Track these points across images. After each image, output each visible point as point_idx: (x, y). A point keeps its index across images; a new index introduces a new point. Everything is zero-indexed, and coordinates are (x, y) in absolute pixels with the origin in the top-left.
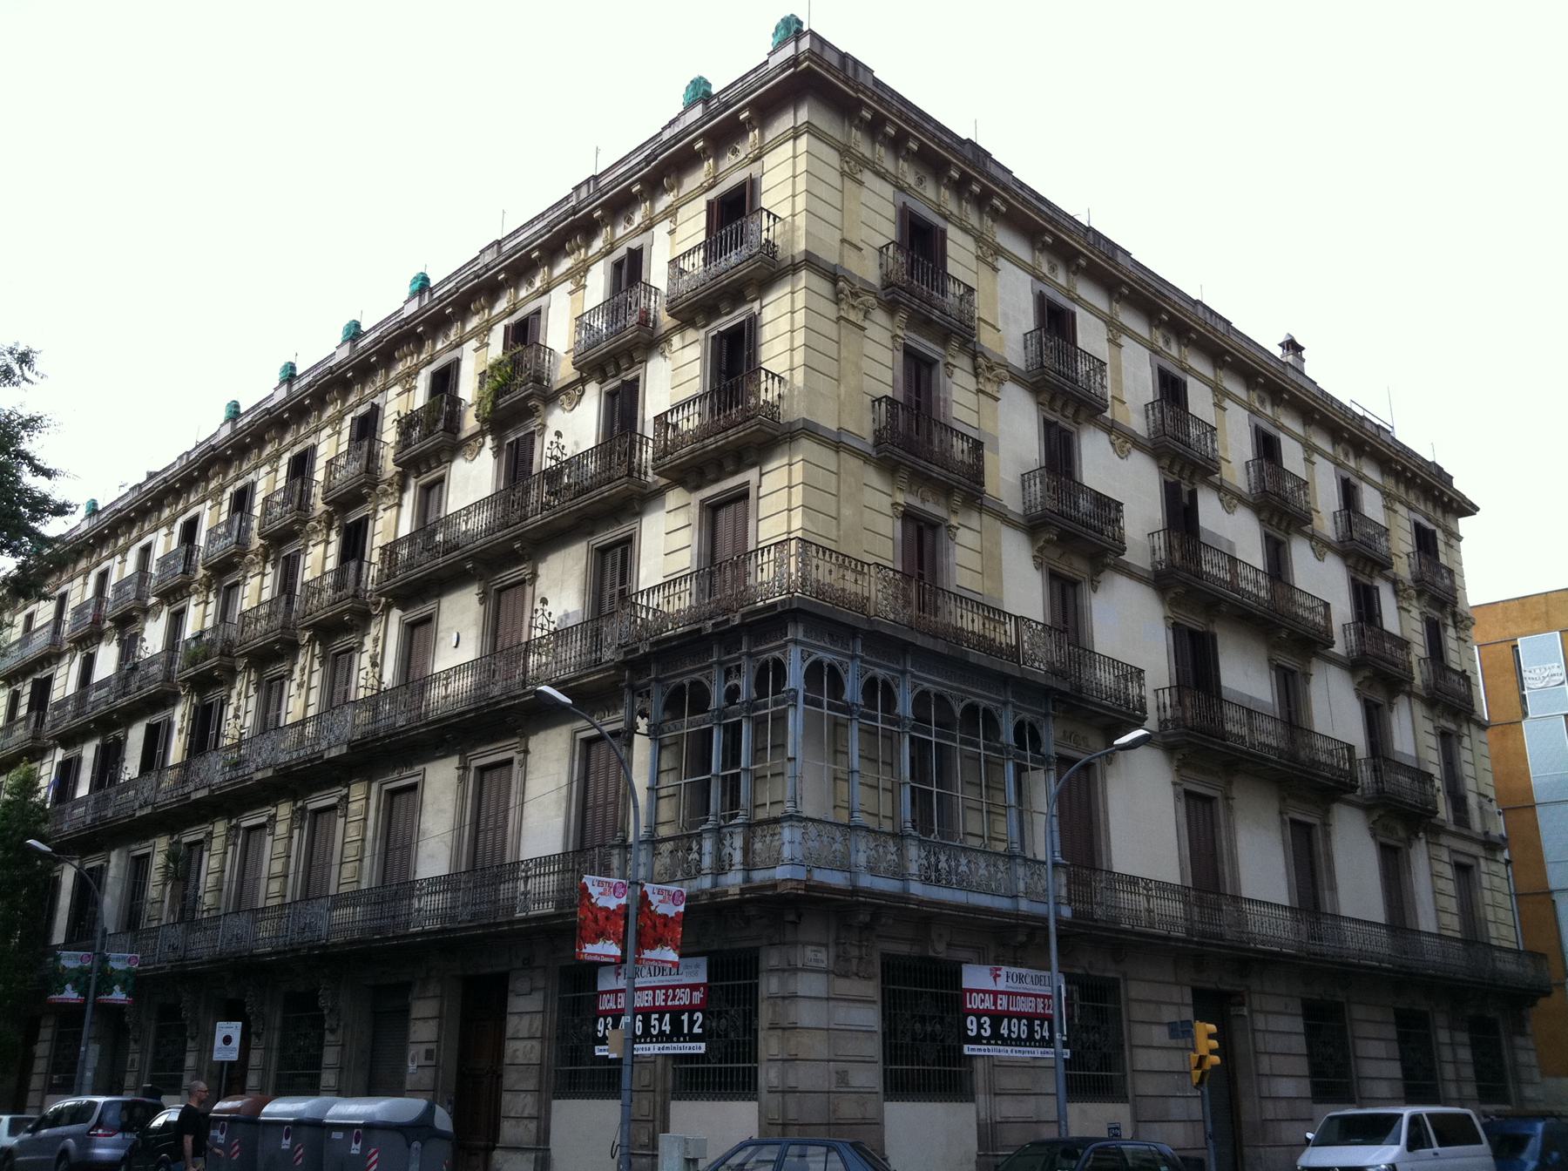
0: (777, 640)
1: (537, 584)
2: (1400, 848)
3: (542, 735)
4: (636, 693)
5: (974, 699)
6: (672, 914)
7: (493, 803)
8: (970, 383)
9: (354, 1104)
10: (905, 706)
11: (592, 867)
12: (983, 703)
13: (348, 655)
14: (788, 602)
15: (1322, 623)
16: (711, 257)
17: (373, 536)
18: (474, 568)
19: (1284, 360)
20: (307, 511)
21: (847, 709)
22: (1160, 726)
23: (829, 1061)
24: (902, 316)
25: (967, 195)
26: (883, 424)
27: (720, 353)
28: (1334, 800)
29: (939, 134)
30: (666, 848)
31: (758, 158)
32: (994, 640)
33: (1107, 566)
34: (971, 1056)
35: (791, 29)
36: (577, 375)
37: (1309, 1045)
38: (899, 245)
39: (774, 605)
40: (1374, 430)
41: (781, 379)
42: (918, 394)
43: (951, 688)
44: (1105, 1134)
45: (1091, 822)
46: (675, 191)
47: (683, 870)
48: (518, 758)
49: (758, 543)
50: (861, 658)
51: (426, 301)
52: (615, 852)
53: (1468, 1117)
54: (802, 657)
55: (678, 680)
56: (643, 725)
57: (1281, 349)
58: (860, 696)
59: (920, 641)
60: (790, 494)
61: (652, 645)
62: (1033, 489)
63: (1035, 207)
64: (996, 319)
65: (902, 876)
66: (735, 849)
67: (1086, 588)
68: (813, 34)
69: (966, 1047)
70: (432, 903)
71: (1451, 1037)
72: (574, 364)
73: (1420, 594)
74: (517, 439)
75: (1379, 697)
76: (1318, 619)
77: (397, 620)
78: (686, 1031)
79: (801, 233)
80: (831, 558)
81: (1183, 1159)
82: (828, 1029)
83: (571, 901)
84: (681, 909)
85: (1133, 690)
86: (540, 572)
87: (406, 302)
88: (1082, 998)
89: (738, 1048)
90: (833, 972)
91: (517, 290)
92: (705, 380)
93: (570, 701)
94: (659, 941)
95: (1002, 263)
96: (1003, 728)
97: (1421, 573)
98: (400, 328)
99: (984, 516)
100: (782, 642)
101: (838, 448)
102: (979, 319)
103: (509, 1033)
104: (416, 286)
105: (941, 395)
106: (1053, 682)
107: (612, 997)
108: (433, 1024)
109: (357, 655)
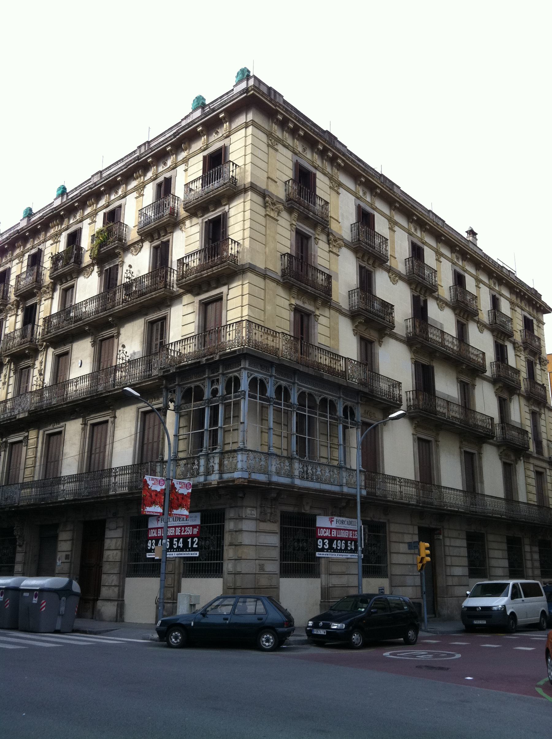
0: (236, 368)
1: (120, 338)
2: (512, 464)
3: (122, 410)
4: (168, 391)
5: (326, 396)
6: (186, 493)
7: (99, 441)
8: (326, 247)
9: (35, 580)
10: (294, 398)
11: (147, 471)
12: (330, 398)
13: (27, 370)
14: (242, 349)
15: (481, 361)
16: (205, 183)
17: (39, 312)
18: (89, 330)
19: (468, 239)
20: (6, 299)
21: (268, 400)
22: (407, 408)
23: (256, 560)
24: (295, 215)
25: (326, 157)
26: (286, 266)
27: (209, 232)
28: (484, 443)
29: (313, 128)
30: (182, 463)
31: (228, 136)
32: (335, 368)
33: (386, 334)
34: (319, 557)
35: (245, 74)
36: (139, 238)
37: (469, 552)
38: (294, 181)
39: (235, 351)
40: (507, 273)
41: (238, 244)
42: (302, 252)
43: (316, 391)
44: (377, 592)
45: (375, 451)
46: (188, 150)
47: (190, 473)
48: (111, 420)
49: (227, 321)
50: (275, 376)
51: (65, 200)
52: (158, 464)
53: (538, 584)
54: (248, 376)
55: (189, 385)
56: (172, 405)
57: (467, 234)
58: (274, 394)
59: (301, 369)
60: (242, 299)
61: (177, 368)
62: (353, 298)
63: (358, 164)
64: (338, 217)
65: (292, 477)
66: (215, 464)
67: (376, 344)
68: (255, 78)
69: (317, 553)
70: (69, 487)
71: (531, 549)
72: (138, 233)
73: (525, 349)
74: (110, 268)
75: (505, 396)
76: (480, 360)
77: (52, 353)
78: (190, 546)
79: (248, 174)
80: (262, 330)
81: (414, 603)
82: (256, 545)
83: (136, 487)
84: (190, 491)
85: (397, 392)
86: (121, 332)
87: (55, 199)
88: (369, 531)
89: (214, 554)
90: (259, 519)
91: (110, 195)
92: (202, 242)
93: (139, 395)
94: (180, 506)
95: (341, 190)
96: (338, 409)
97: (526, 339)
98: (52, 212)
99: (331, 310)
100: (238, 368)
101: (265, 277)
102: (331, 217)
103: (106, 548)
104: (60, 192)
105: (313, 253)
106: (361, 388)
107: (155, 531)
108: (69, 543)
109: (32, 370)
